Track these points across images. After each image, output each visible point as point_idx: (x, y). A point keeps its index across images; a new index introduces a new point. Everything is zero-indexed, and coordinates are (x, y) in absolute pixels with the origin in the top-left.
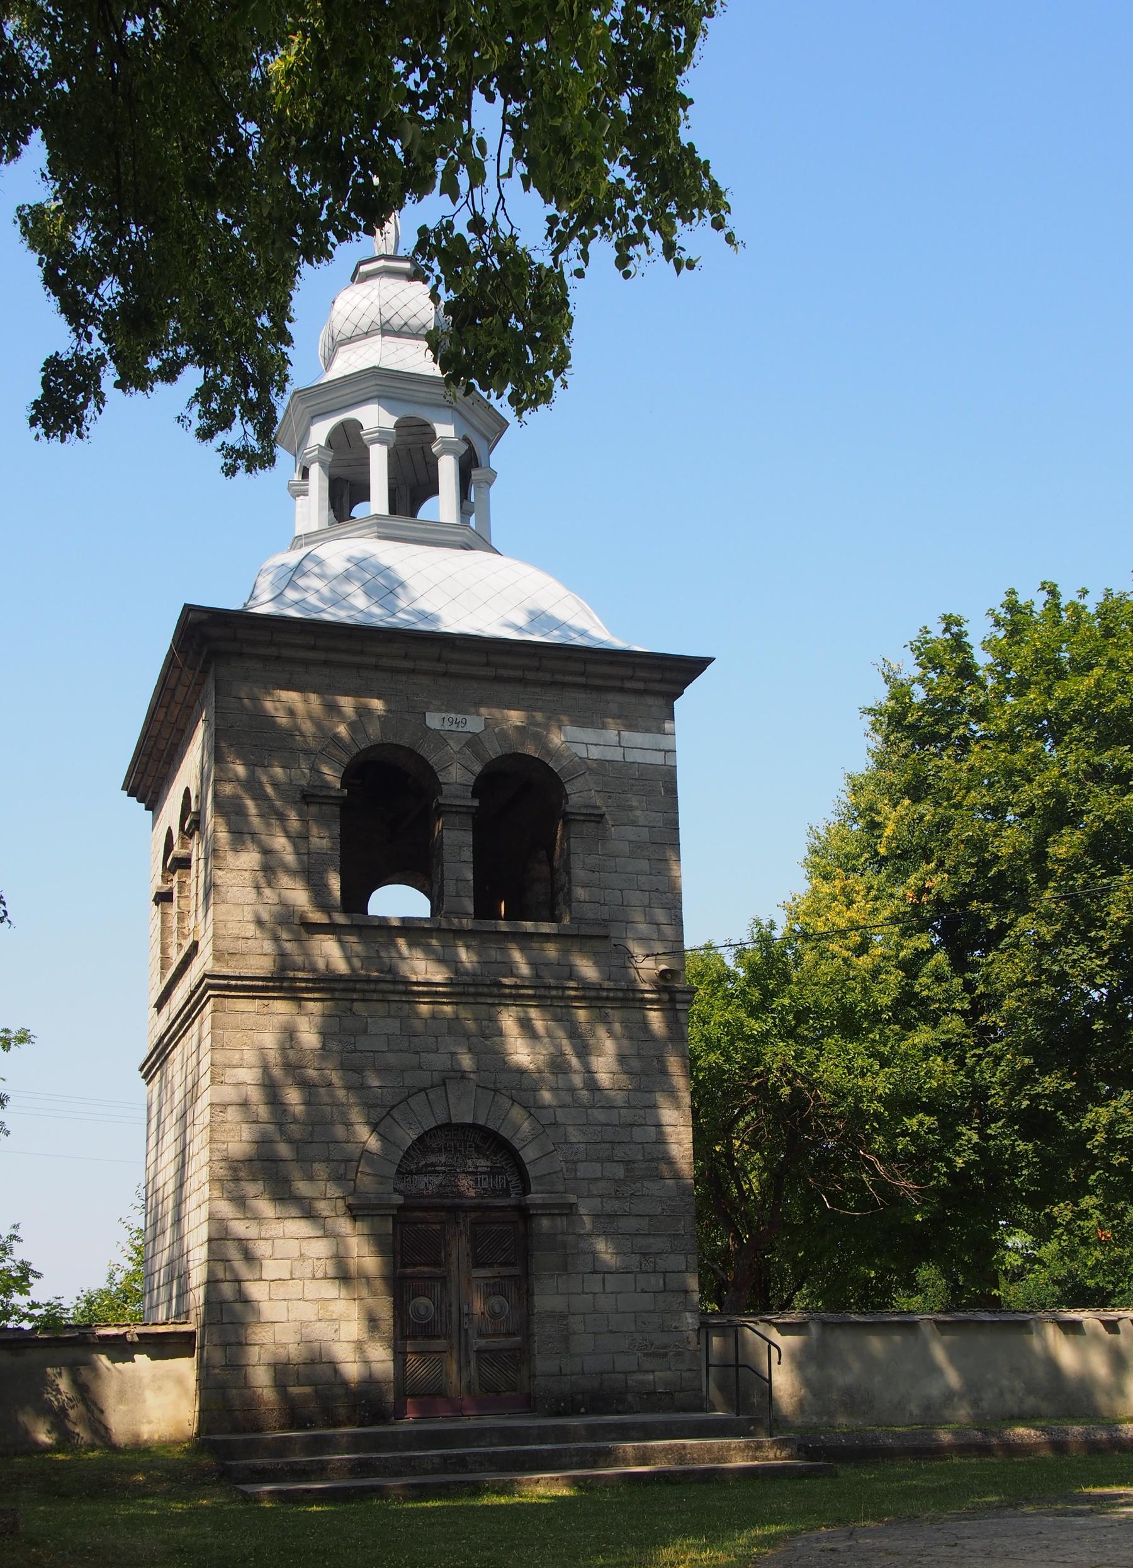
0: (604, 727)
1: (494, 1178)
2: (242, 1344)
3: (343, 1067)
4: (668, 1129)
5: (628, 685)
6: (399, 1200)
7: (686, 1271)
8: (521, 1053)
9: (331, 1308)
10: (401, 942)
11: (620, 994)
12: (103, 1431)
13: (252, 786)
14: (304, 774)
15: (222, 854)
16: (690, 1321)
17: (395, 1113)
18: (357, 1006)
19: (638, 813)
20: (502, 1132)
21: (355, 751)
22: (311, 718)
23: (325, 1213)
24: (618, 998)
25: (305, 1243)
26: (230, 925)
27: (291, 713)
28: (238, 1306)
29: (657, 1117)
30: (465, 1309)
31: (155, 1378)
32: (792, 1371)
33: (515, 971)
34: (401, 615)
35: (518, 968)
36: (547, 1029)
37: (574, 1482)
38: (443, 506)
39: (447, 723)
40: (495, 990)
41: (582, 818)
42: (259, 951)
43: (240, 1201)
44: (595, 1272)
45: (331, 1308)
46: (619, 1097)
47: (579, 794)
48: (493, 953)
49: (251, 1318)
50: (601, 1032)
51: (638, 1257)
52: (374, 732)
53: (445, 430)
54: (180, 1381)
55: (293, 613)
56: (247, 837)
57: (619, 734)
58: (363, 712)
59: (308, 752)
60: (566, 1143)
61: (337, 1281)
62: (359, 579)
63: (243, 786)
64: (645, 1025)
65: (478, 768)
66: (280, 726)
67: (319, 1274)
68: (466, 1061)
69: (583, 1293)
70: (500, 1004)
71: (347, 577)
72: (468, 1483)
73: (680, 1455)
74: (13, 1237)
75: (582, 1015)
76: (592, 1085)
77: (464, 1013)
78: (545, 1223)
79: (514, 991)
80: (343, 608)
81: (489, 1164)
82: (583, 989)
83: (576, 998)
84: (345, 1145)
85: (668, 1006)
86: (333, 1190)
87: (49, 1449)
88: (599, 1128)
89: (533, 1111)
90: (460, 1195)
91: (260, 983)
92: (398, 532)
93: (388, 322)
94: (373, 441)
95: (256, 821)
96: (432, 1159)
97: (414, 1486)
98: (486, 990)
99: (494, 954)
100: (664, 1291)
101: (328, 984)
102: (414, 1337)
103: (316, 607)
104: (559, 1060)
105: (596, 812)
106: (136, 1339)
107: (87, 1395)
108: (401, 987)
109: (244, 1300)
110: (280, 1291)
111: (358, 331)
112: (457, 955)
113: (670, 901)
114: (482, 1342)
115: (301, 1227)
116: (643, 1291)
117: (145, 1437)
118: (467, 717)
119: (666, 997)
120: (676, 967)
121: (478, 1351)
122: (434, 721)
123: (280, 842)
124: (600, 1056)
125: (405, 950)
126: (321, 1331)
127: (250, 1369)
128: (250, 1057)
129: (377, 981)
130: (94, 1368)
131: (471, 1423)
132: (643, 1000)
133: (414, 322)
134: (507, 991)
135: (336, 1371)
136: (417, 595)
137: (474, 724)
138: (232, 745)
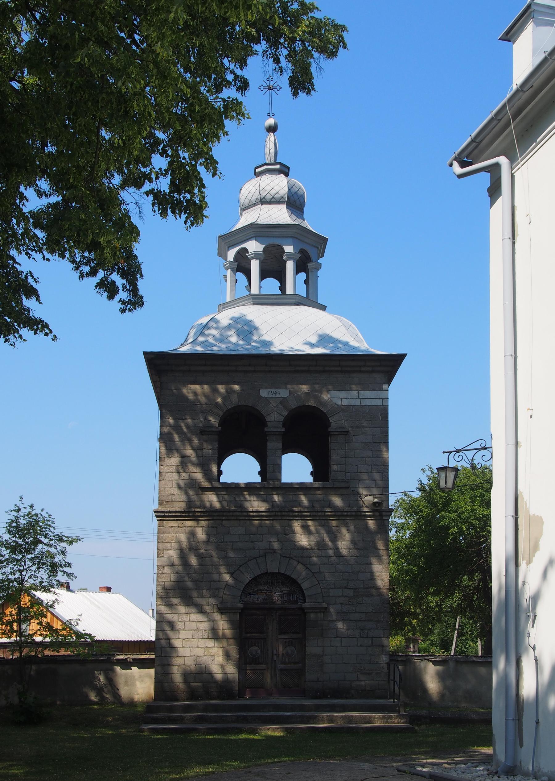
0: (351, 389)
1: (290, 596)
2: (169, 665)
3: (217, 549)
4: (377, 574)
5: (363, 369)
6: (241, 606)
7: (384, 637)
8: (303, 540)
9: (210, 651)
10: (246, 493)
11: (354, 513)
12: (118, 697)
13: (177, 428)
14: (201, 422)
15: (163, 459)
16: (384, 659)
17: (241, 569)
18: (224, 522)
19: (367, 429)
20: (293, 576)
21: (225, 409)
22: (205, 396)
23: (208, 611)
24: (352, 515)
25: (198, 624)
26: (166, 489)
27: (195, 394)
28: (168, 649)
29: (371, 568)
30: (275, 652)
31: (140, 677)
32: (439, 682)
33: (301, 504)
34: (254, 344)
35: (303, 503)
36: (316, 530)
37: (286, 730)
38: (294, 282)
39: (270, 394)
40: (291, 514)
41: (337, 433)
42: (180, 500)
43: (170, 605)
44: (337, 637)
45: (210, 651)
46: (352, 561)
47: (335, 422)
48: (291, 497)
49: (175, 655)
50: (344, 530)
51: (359, 631)
52: (234, 399)
53: (289, 249)
54: (150, 677)
55: (199, 349)
56: (175, 451)
57: (358, 392)
58: (230, 392)
59: (203, 411)
60: (324, 580)
61: (213, 640)
62: (235, 328)
63: (173, 429)
64: (367, 526)
65: (285, 413)
66: (191, 400)
67: (205, 636)
68: (276, 545)
69: (331, 646)
70: (293, 520)
71: (229, 327)
72: (237, 729)
73: (350, 719)
74: (79, 620)
75: (334, 523)
76: (338, 553)
77: (276, 524)
78: (312, 616)
79: (300, 514)
80: (225, 343)
81: (288, 589)
82: (335, 511)
83: (331, 516)
84: (218, 582)
85: (379, 518)
86: (212, 601)
87: (95, 703)
88: (341, 574)
89: (308, 566)
90: (274, 603)
91: (179, 514)
92: (262, 301)
93: (264, 198)
94: (253, 258)
95: (178, 444)
96: (260, 588)
97: (212, 729)
98: (286, 514)
99: (291, 497)
100: (372, 646)
101: (210, 513)
102: (251, 663)
103: (211, 344)
104: (322, 543)
105: (344, 430)
106: (132, 661)
107: (111, 682)
108: (245, 514)
109: (172, 647)
110: (187, 643)
111: (251, 203)
112: (273, 498)
113: (383, 470)
114: (282, 666)
115: (199, 617)
116: (361, 646)
117: (136, 700)
118: (280, 390)
119: (377, 514)
120: (384, 499)
121: (281, 670)
122: (264, 393)
123: (189, 452)
124: (343, 541)
125: (247, 497)
126: (206, 660)
127: (174, 675)
128: (175, 545)
129: (234, 511)
130: (113, 671)
131: (273, 700)
132: (366, 515)
133: (277, 196)
134: (297, 514)
135: (212, 677)
136: (263, 333)
137: (284, 393)
138: (168, 411)
